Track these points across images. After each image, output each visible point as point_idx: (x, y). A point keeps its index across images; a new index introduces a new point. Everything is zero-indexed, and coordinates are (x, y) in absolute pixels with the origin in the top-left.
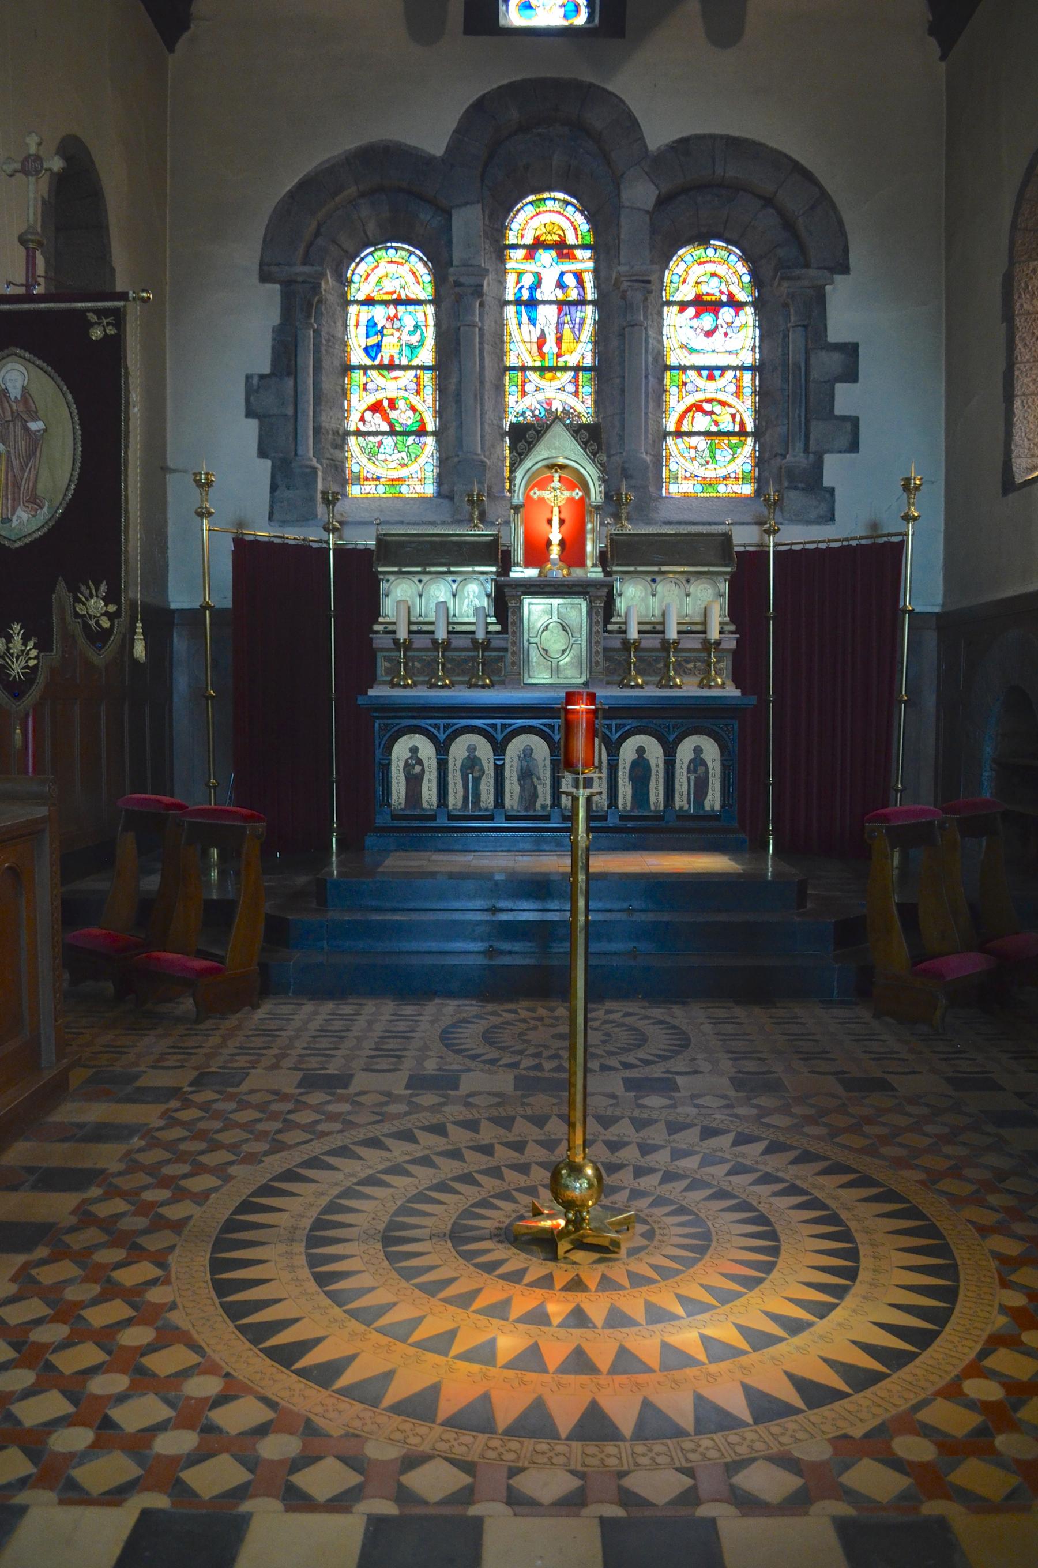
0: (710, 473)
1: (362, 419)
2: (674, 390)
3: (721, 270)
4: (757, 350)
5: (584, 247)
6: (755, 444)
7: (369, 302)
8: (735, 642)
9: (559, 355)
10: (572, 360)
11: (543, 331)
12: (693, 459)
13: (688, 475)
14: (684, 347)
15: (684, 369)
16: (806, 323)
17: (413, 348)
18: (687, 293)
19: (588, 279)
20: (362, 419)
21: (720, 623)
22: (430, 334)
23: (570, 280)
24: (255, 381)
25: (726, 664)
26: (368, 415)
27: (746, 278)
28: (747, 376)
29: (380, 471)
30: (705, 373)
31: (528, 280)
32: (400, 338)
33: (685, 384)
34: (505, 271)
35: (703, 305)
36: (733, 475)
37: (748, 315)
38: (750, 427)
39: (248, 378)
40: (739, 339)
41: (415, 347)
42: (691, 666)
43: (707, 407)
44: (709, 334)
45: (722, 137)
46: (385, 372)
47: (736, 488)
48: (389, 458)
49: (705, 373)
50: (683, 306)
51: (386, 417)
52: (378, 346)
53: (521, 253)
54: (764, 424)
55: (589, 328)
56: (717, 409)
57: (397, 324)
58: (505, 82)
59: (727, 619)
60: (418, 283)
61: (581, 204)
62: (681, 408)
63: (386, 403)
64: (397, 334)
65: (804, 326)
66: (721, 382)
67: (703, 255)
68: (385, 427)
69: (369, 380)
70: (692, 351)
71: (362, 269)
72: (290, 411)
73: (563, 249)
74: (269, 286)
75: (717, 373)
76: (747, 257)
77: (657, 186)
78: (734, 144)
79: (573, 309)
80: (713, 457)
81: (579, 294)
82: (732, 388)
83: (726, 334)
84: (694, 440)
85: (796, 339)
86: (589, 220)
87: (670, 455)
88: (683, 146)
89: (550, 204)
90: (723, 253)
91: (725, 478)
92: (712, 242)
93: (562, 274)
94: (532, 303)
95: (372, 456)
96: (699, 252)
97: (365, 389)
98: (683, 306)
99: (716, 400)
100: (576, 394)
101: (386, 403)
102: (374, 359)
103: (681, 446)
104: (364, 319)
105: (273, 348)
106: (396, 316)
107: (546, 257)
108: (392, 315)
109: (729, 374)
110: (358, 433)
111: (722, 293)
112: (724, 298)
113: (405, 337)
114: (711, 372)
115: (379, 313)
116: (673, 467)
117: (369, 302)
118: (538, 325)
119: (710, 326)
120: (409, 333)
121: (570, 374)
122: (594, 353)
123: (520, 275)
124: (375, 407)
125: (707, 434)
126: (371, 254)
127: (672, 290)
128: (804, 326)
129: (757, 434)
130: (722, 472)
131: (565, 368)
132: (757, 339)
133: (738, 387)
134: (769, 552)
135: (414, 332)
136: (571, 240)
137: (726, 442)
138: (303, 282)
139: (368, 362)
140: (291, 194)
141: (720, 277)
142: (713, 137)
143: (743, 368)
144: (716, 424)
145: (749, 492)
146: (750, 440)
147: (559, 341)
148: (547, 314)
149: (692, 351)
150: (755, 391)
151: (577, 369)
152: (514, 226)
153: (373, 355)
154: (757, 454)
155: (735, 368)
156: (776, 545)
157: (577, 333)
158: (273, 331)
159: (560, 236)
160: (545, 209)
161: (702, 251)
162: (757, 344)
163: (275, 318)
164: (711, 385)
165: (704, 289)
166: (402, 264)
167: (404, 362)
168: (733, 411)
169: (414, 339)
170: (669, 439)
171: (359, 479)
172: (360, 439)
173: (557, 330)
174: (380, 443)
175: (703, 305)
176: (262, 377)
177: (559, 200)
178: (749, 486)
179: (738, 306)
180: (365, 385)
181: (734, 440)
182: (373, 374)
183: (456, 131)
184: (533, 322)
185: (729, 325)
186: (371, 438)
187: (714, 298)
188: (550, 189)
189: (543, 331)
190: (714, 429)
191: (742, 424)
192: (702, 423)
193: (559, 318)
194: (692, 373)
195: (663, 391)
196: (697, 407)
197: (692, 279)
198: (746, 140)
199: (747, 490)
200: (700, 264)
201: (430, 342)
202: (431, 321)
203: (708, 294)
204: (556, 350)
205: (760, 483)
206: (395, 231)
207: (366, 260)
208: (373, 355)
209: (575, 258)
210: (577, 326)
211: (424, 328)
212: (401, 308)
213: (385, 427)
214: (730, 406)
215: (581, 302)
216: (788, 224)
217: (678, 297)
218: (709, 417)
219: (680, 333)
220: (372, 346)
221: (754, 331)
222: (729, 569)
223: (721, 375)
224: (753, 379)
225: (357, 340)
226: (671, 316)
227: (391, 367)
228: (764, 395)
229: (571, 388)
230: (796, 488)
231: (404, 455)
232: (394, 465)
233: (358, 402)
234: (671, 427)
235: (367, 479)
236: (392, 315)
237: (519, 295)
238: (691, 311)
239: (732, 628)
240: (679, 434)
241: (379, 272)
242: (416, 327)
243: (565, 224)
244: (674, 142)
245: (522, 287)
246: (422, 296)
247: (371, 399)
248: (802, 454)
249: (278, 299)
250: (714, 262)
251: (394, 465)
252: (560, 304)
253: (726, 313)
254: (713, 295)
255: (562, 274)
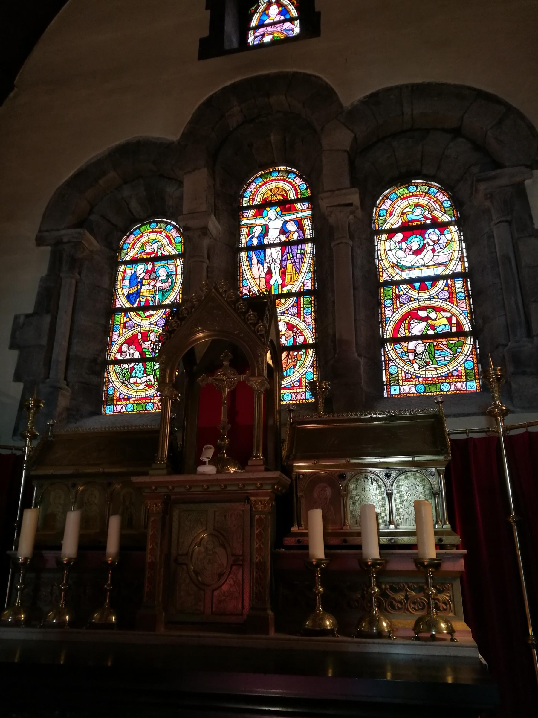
0: (431, 374)
1: (120, 351)
2: (388, 303)
3: (424, 201)
4: (466, 260)
5: (301, 200)
6: (474, 342)
7: (134, 261)
8: (462, 561)
9: (283, 285)
10: (295, 288)
11: (269, 268)
12: (411, 362)
13: (408, 376)
14: (394, 266)
15: (397, 284)
16: (509, 218)
17: (164, 291)
18: (394, 222)
19: (307, 223)
20: (120, 351)
21: (436, 533)
22: (179, 279)
23: (291, 227)
24: (22, 320)
25: (453, 596)
26: (125, 348)
27: (448, 204)
28: (459, 284)
29: (132, 393)
30: (417, 285)
31: (257, 231)
32: (154, 286)
33: (398, 296)
34: (239, 227)
35: (409, 229)
36: (455, 373)
37: (453, 233)
38: (467, 327)
39: (16, 317)
40: (447, 252)
41: (167, 291)
42: (400, 596)
43: (422, 314)
44: (417, 252)
45: (407, 86)
46: (141, 313)
47: (459, 385)
48: (139, 381)
49: (417, 285)
50: (391, 233)
51: (139, 348)
52: (138, 293)
53: (251, 212)
54: (480, 321)
55: (308, 259)
56: (433, 315)
57: (153, 275)
58: (229, 83)
59: (447, 526)
60: (171, 243)
61: (300, 171)
62: (397, 317)
63: (139, 337)
64: (152, 283)
65: (507, 221)
66: (434, 291)
67: (407, 192)
68: (137, 355)
69: (128, 319)
70: (403, 268)
71: (131, 240)
72: (44, 341)
73: (286, 205)
74: (43, 248)
75: (429, 283)
76: (445, 188)
77: (352, 131)
78: (420, 91)
79: (294, 248)
80: (433, 357)
81: (299, 236)
82: (446, 295)
83: (434, 250)
84: (411, 345)
85: (501, 234)
86: (306, 181)
87: (389, 359)
88: (374, 99)
89: (275, 174)
90: (423, 188)
91: (447, 377)
92: (413, 181)
93: (285, 222)
94: (261, 247)
95: (125, 382)
96: (403, 191)
97: (124, 327)
98: (391, 233)
99: (430, 307)
100: (298, 315)
101: (139, 337)
102: (133, 303)
103: (400, 351)
104: (129, 272)
105: (39, 294)
106: (153, 269)
107: (271, 213)
108: (149, 269)
109: (441, 284)
110: (116, 362)
111: (426, 218)
112: (428, 222)
113: (159, 285)
114: (423, 283)
115: (140, 268)
116: (393, 370)
117: (134, 261)
118: (266, 265)
119: (421, 250)
120: (162, 282)
121: (293, 299)
122: (313, 279)
123: (251, 228)
124: (131, 341)
125: (423, 337)
126: (139, 228)
127: (380, 222)
128: (507, 221)
129: (475, 333)
130: (443, 371)
131: (289, 295)
132: (464, 251)
133: (450, 293)
134: (499, 439)
135: (165, 281)
136: (292, 195)
137: (445, 343)
138: (69, 242)
139: (128, 305)
140: (68, 183)
141: (422, 206)
142: (399, 88)
143: (454, 276)
144: (433, 327)
145: (474, 388)
146: (469, 340)
147: (283, 274)
148: (274, 253)
149: (403, 268)
150: (468, 296)
151: (299, 294)
152: (247, 194)
153: (133, 300)
154: (478, 351)
155: (444, 277)
156: (505, 430)
157: (298, 266)
158: (41, 280)
159: (283, 195)
160: (271, 179)
161: (405, 189)
162: (465, 255)
163: (43, 270)
164: (424, 295)
165: (410, 217)
166: (160, 232)
167: (157, 303)
168: (449, 315)
169: (166, 285)
170: (389, 347)
171: (113, 400)
172: (117, 367)
173: (281, 266)
174: (133, 368)
175: (409, 229)
176: (27, 316)
177: (283, 171)
178: (473, 383)
179: (442, 227)
180: (125, 323)
181: (453, 341)
182: (132, 314)
183: (190, 123)
184: (261, 262)
185: (436, 242)
186: (126, 366)
187: (419, 223)
188: (276, 165)
189: (269, 268)
190: (431, 332)
191: (459, 325)
192: (418, 328)
193: (282, 256)
194: (404, 287)
195: (379, 304)
196: (412, 315)
197: (397, 211)
198: (429, 85)
199: (472, 386)
200: (403, 199)
201: (178, 287)
202: (180, 271)
203: (413, 221)
204: (280, 281)
205: (484, 375)
206: (155, 210)
207: (135, 233)
208: (133, 300)
209: (295, 209)
210: (298, 261)
211: (174, 276)
212: (157, 263)
213: (137, 355)
214: (445, 311)
215: (302, 241)
216: (479, 147)
217: (387, 226)
218: (424, 323)
219: (393, 255)
220: (133, 294)
221: (460, 244)
222: (441, 457)
223: (432, 285)
224: (465, 284)
225: (123, 288)
226: (383, 243)
227: (147, 308)
228: (476, 296)
229: (294, 311)
230: (524, 373)
231: (151, 377)
232: (142, 387)
233: (119, 337)
234: (388, 335)
235: (119, 400)
236: (149, 269)
237: (249, 243)
238: (399, 236)
239: (456, 539)
240: (396, 340)
241: (143, 240)
242: (168, 276)
243: (288, 187)
244: (365, 98)
245: (253, 237)
246: (170, 250)
247: (129, 334)
248: (525, 339)
249: (48, 256)
250: (416, 196)
251: (142, 387)
252: (282, 245)
253: (432, 234)
254: (418, 220)
255: (285, 222)
